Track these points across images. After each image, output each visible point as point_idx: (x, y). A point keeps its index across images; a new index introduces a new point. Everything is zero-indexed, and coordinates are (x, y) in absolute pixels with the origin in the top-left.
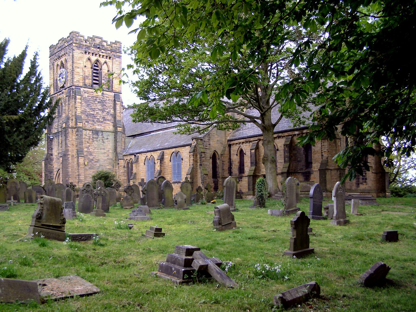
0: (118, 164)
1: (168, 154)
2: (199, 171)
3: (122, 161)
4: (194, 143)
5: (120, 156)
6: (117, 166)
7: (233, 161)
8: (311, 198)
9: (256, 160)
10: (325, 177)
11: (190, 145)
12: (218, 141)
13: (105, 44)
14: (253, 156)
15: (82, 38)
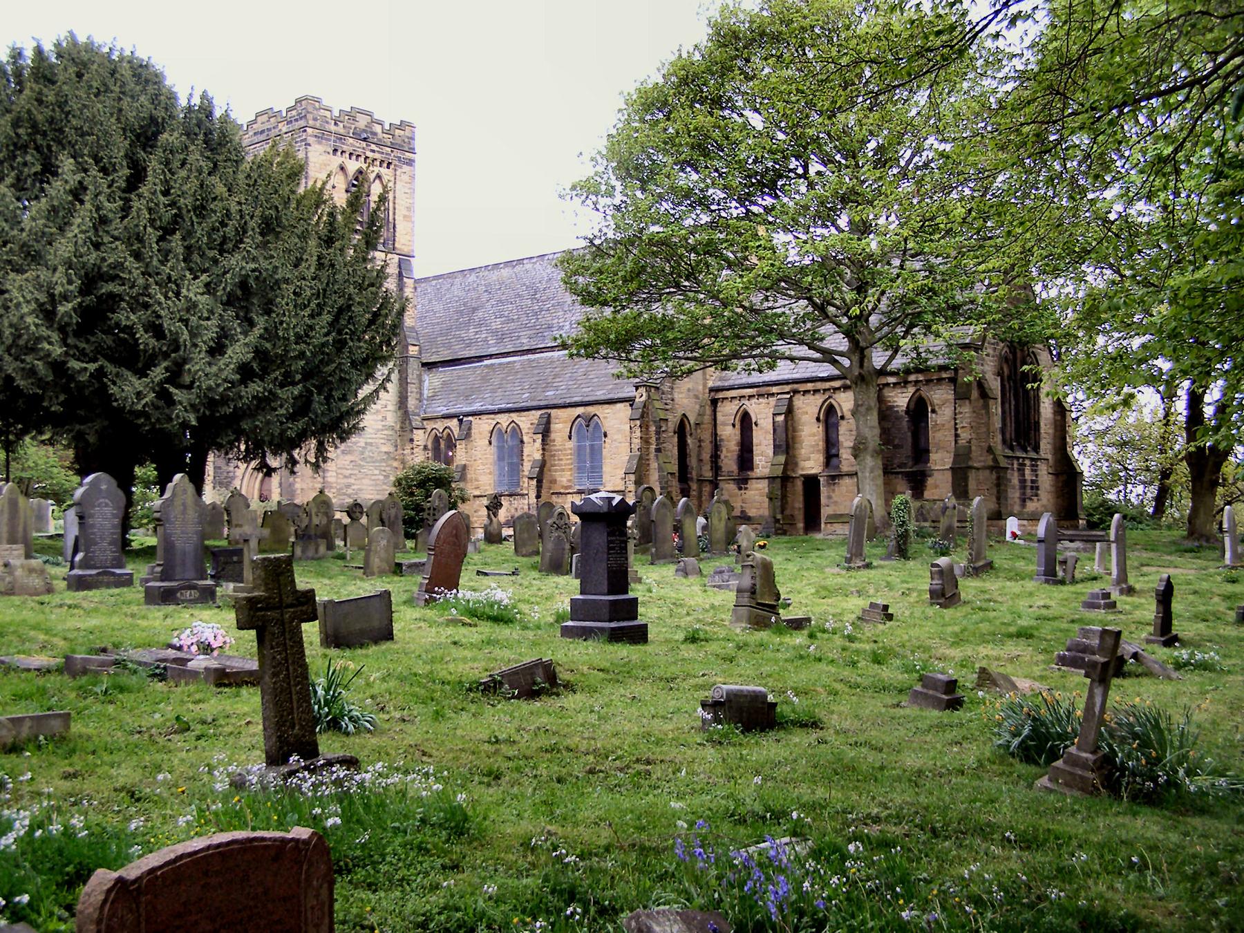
0: (412, 440)
1: (562, 422)
2: (654, 465)
3: (421, 432)
4: (641, 396)
5: (416, 421)
6: (408, 446)
7: (721, 440)
8: (1039, 541)
9: (787, 441)
10: (967, 485)
11: (630, 401)
12: (689, 390)
13: (378, 129)
14: (780, 430)
15: (328, 114)
